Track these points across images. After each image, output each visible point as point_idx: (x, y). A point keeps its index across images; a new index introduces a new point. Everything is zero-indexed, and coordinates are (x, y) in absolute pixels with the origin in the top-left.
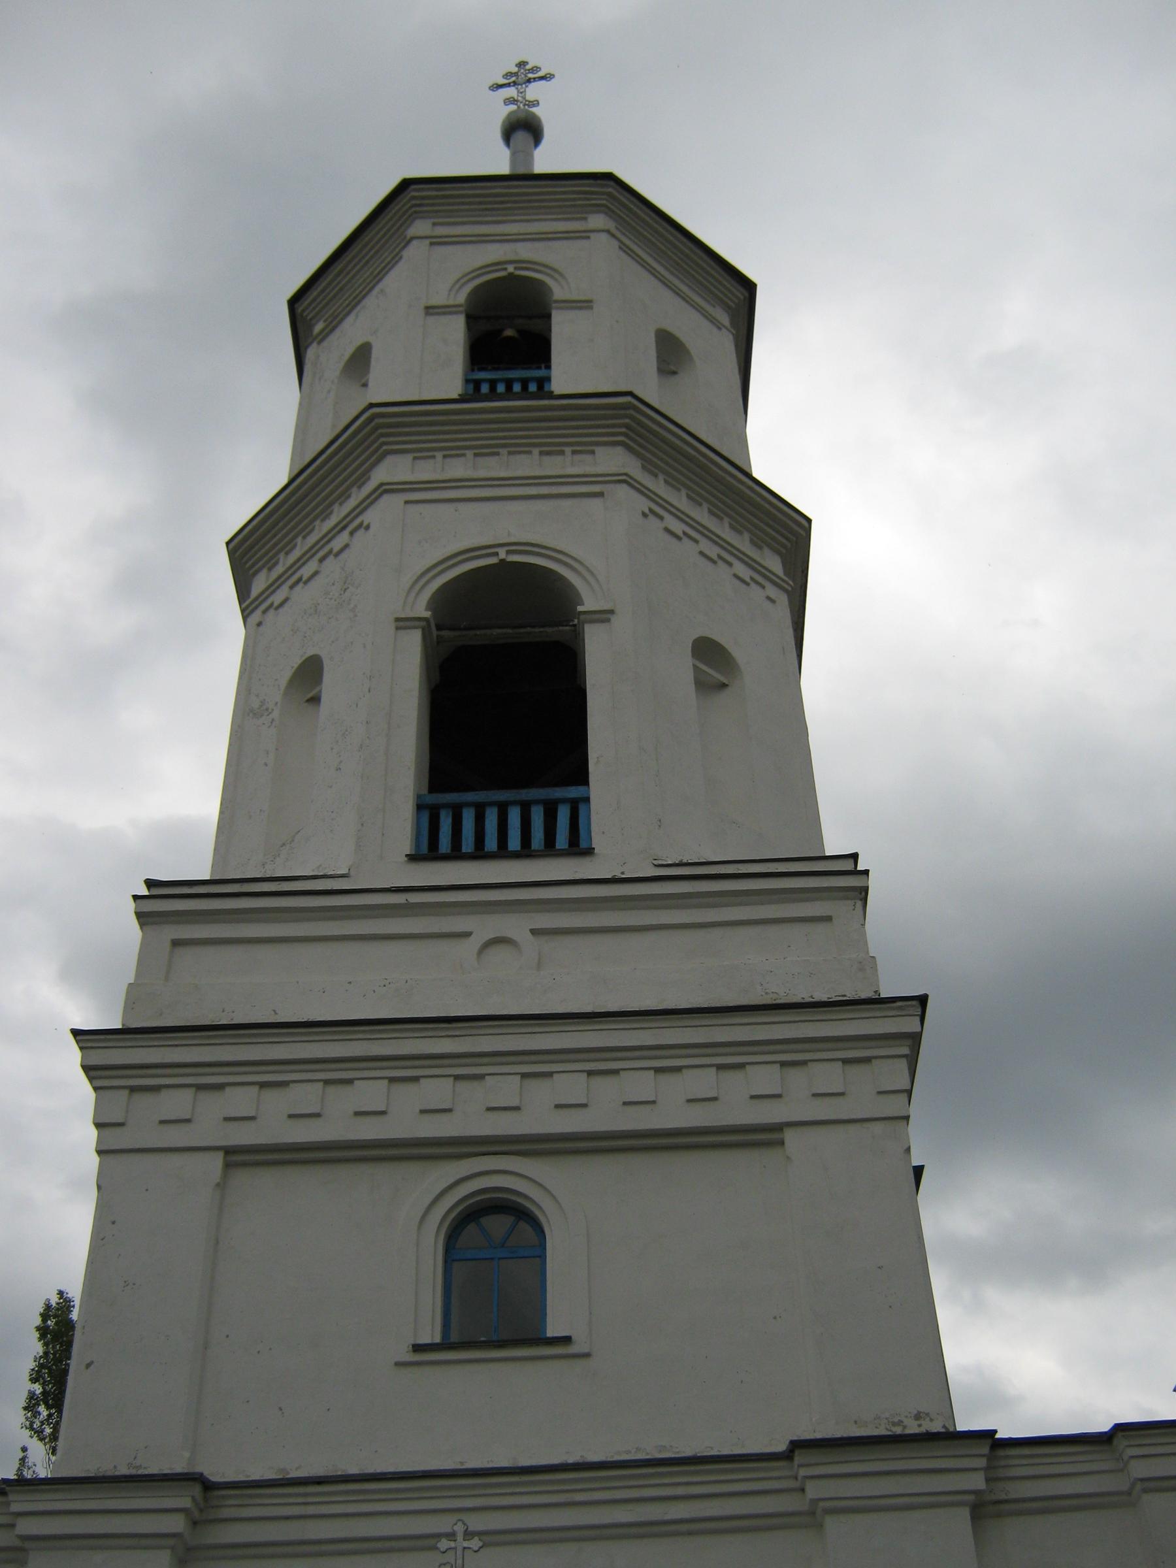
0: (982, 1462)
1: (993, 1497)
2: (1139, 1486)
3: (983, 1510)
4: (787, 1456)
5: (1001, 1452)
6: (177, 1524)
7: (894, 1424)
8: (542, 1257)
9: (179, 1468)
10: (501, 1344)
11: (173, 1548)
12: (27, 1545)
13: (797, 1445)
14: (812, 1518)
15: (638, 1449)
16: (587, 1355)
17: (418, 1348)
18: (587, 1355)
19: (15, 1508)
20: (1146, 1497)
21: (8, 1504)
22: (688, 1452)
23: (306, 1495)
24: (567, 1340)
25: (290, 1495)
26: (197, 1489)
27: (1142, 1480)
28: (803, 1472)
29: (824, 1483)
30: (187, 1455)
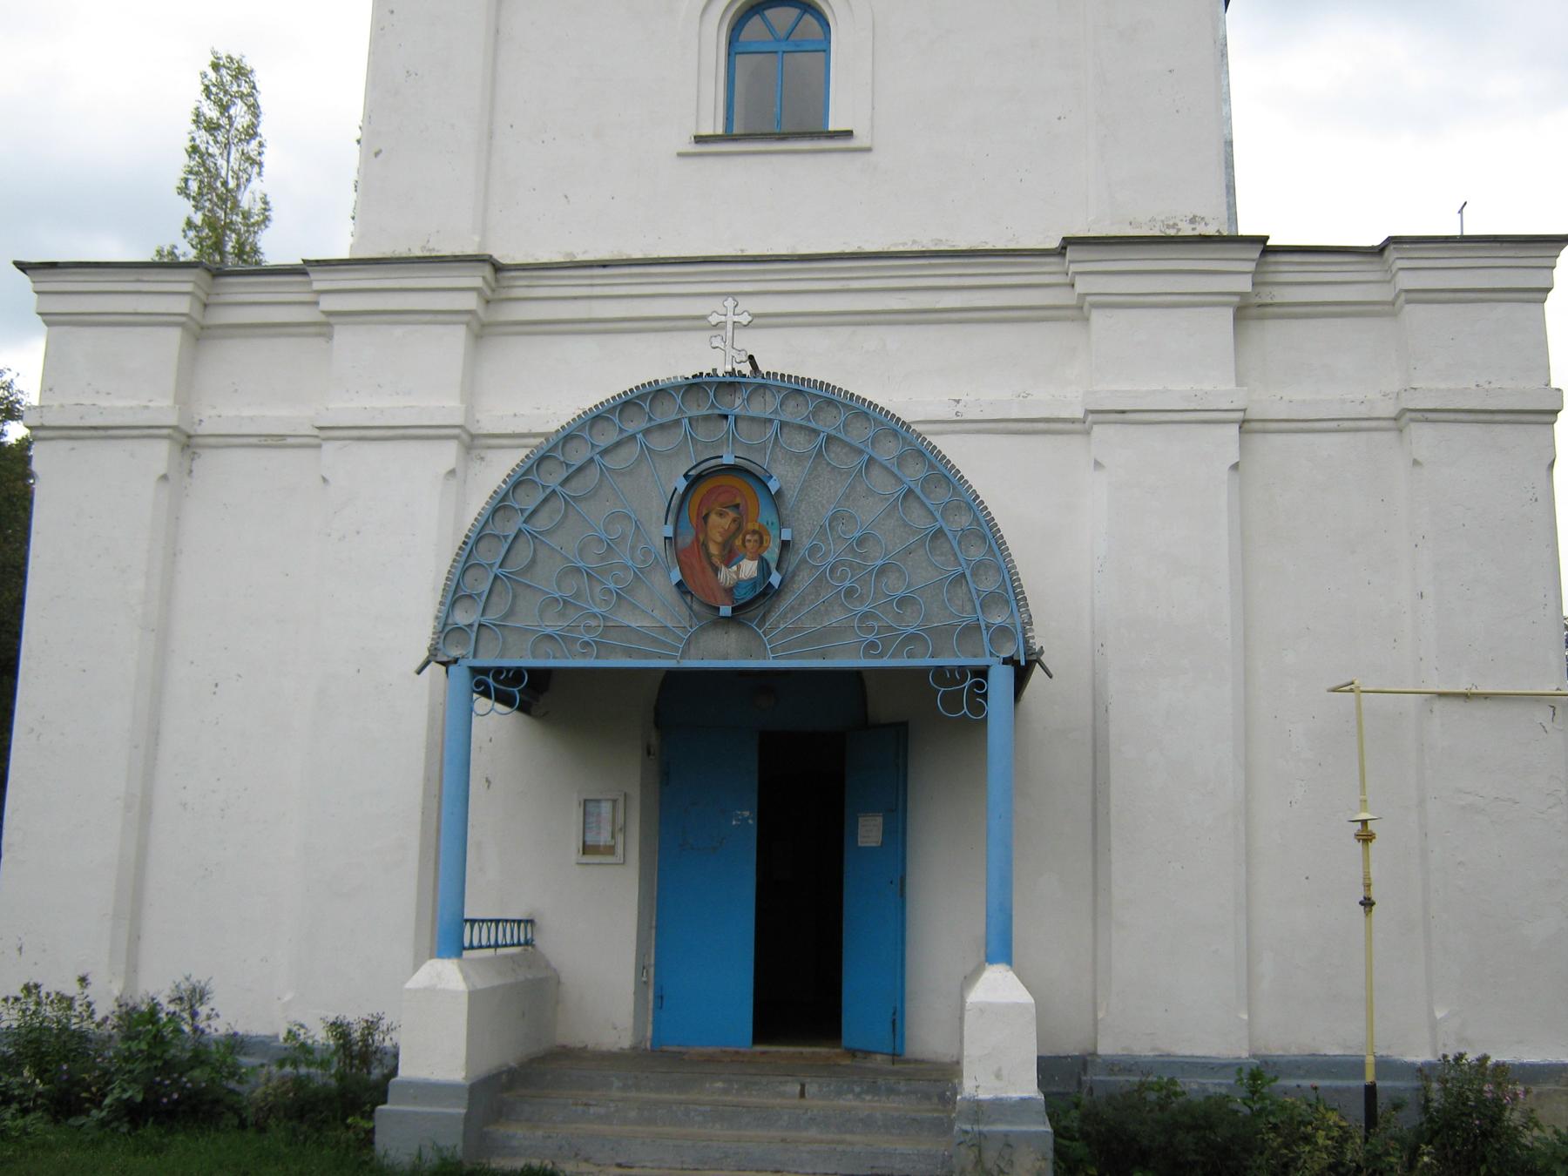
0: (1251, 266)
1: (1258, 300)
2: (1403, 297)
3: (1246, 312)
4: (1061, 251)
5: (1271, 258)
6: (470, 302)
7: (1168, 227)
8: (826, 51)
9: (471, 250)
10: (783, 137)
11: (468, 324)
12: (332, 320)
13: (1068, 242)
14: (1079, 312)
15: (914, 242)
16: (868, 150)
17: (699, 139)
18: (868, 150)
19: (317, 286)
20: (1408, 307)
21: (310, 283)
22: (963, 246)
23: (592, 277)
24: (848, 134)
25: (563, 278)
26: (487, 271)
27: (1407, 291)
28: (1073, 268)
29: (1095, 278)
30: (477, 239)
